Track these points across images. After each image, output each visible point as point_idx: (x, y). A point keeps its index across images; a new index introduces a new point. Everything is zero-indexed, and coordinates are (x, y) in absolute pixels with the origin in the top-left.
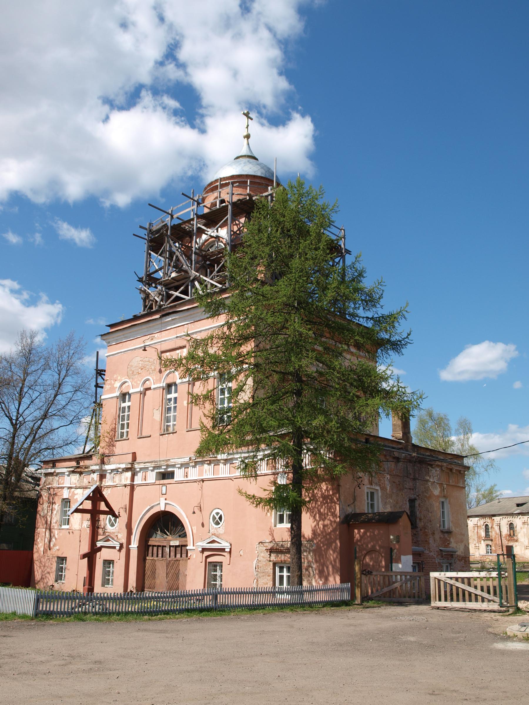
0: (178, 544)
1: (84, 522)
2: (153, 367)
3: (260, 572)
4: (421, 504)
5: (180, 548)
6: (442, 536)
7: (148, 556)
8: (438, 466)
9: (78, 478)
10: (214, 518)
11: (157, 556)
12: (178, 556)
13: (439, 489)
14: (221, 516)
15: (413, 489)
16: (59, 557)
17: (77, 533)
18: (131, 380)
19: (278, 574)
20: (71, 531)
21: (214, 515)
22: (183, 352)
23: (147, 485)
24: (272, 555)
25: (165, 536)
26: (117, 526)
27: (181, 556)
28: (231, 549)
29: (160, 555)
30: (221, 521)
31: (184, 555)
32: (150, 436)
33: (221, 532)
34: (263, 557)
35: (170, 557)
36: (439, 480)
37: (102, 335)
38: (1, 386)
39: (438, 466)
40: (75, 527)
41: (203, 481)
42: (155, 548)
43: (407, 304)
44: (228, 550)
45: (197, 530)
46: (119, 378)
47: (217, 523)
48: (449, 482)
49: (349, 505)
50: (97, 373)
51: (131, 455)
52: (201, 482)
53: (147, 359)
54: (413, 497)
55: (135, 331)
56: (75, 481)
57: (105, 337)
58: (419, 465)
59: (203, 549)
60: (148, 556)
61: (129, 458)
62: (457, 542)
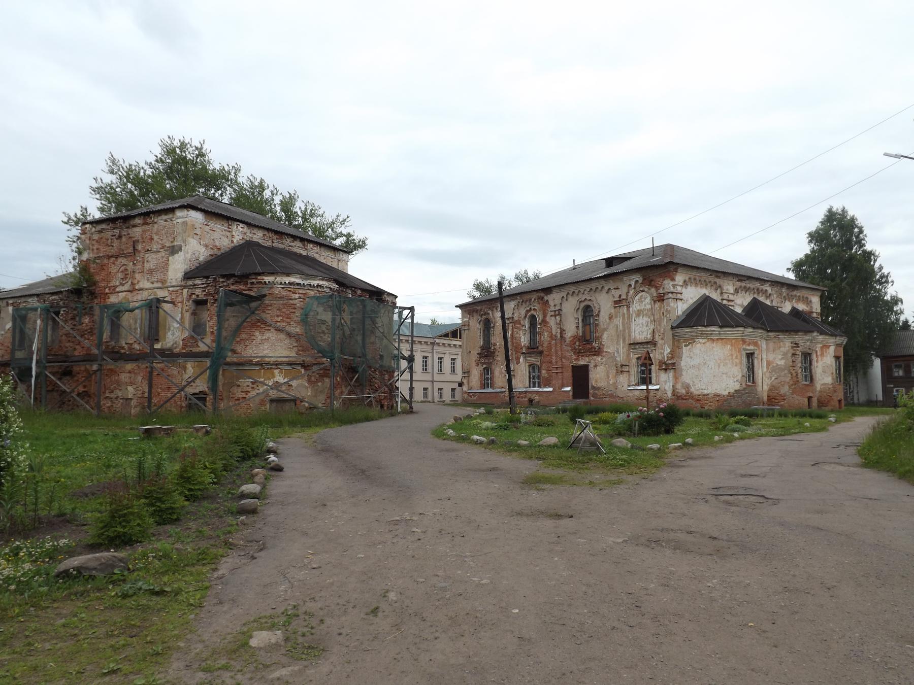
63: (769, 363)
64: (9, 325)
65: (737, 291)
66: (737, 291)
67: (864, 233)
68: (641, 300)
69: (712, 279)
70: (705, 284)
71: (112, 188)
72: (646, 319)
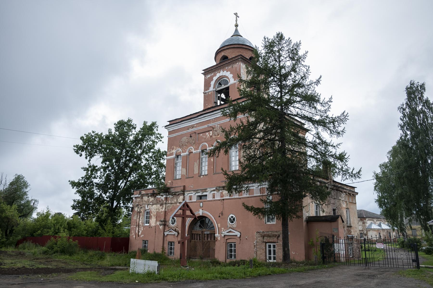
0: (209, 233)
2: (194, 142)
3: (258, 248)
4: (338, 212)
5: (210, 235)
6: (348, 229)
7: (192, 239)
8: (345, 192)
11: (197, 239)
12: (209, 239)
13: (345, 204)
16: (144, 240)
18: (182, 149)
19: (268, 249)
20: (150, 227)
21: (230, 218)
24: (412, 252)
25: (202, 229)
26: (176, 224)
27: (211, 240)
28: (240, 235)
29: (198, 239)
30: (234, 221)
31: (213, 239)
32: (193, 177)
34: (259, 240)
35: (204, 240)
36: (345, 199)
39: (345, 192)
40: (152, 225)
42: (196, 235)
43: (225, 128)
44: (239, 236)
45: (220, 226)
46: (175, 148)
47: (232, 222)
48: (349, 200)
49: (307, 212)
52: (223, 200)
54: (335, 208)
58: (336, 191)
59: (224, 235)
60: (192, 239)
61: (182, 188)
62: (354, 232)
63: (383, 234)
64: (289, 233)
65: (376, 221)
66: (376, 221)
67: (286, 38)
68: (360, 223)
69: (372, 219)
70: (371, 220)
71: (117, 128)
72: (361, 226)
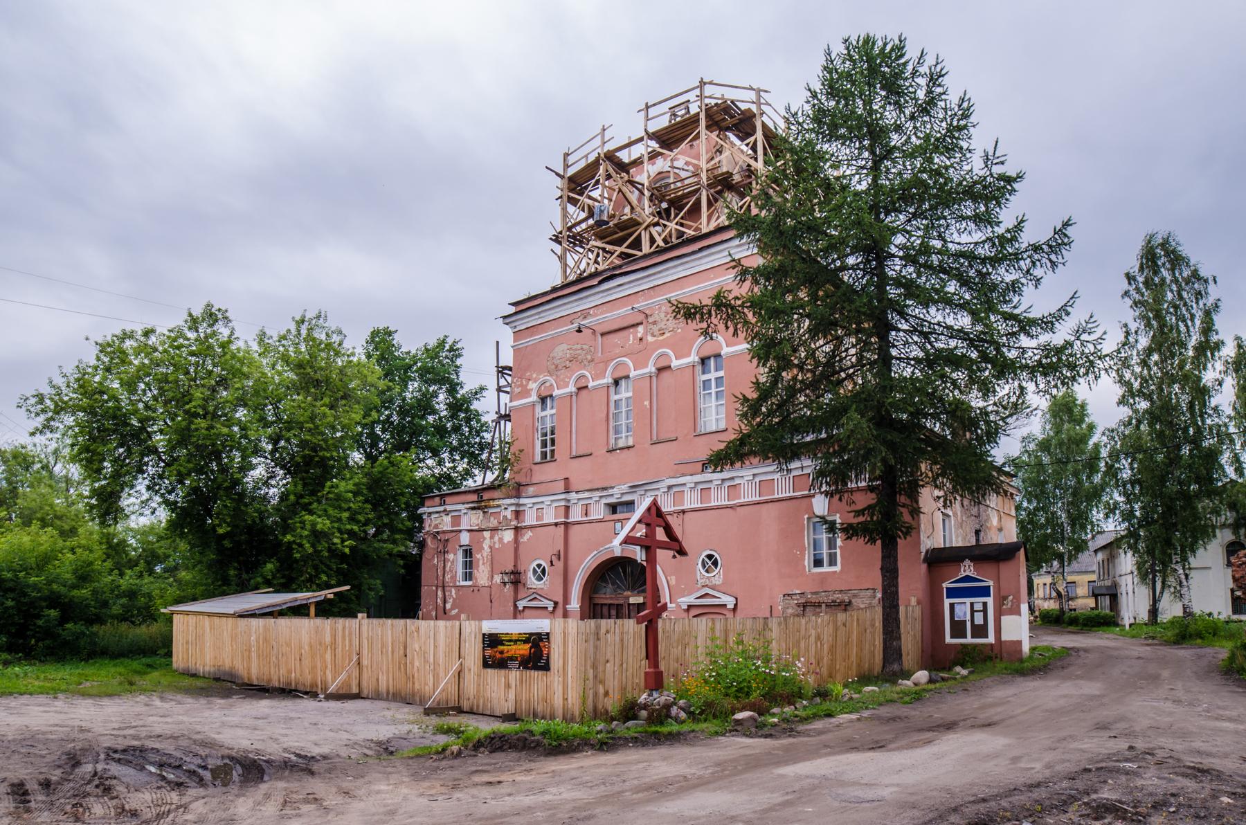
1: (496, 576)
9: (481, 517)
10: (535, 571)
14: (544, 568)
15: (978, 516)
17: (485, 592)
22: (637, 332)
23: (590, 522)
28: (736, 605)
33: (717, 583)
37: (505, 317)
38: (2, 533)
41: (684, 512)
46: (534, 376)
50: (499, 372)
51: (562, 483)
53: (579, 346)
55: (576, 300)
56: (476, 522)
57: (508, 320)
59: (689, 606)
